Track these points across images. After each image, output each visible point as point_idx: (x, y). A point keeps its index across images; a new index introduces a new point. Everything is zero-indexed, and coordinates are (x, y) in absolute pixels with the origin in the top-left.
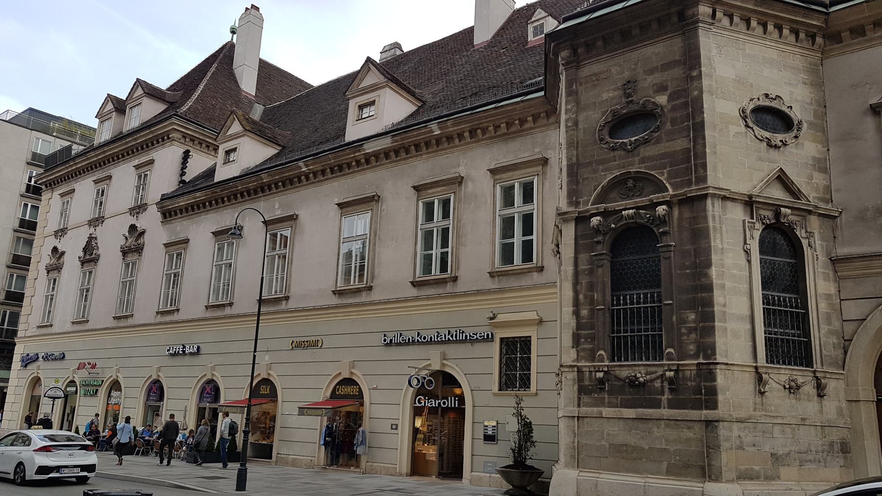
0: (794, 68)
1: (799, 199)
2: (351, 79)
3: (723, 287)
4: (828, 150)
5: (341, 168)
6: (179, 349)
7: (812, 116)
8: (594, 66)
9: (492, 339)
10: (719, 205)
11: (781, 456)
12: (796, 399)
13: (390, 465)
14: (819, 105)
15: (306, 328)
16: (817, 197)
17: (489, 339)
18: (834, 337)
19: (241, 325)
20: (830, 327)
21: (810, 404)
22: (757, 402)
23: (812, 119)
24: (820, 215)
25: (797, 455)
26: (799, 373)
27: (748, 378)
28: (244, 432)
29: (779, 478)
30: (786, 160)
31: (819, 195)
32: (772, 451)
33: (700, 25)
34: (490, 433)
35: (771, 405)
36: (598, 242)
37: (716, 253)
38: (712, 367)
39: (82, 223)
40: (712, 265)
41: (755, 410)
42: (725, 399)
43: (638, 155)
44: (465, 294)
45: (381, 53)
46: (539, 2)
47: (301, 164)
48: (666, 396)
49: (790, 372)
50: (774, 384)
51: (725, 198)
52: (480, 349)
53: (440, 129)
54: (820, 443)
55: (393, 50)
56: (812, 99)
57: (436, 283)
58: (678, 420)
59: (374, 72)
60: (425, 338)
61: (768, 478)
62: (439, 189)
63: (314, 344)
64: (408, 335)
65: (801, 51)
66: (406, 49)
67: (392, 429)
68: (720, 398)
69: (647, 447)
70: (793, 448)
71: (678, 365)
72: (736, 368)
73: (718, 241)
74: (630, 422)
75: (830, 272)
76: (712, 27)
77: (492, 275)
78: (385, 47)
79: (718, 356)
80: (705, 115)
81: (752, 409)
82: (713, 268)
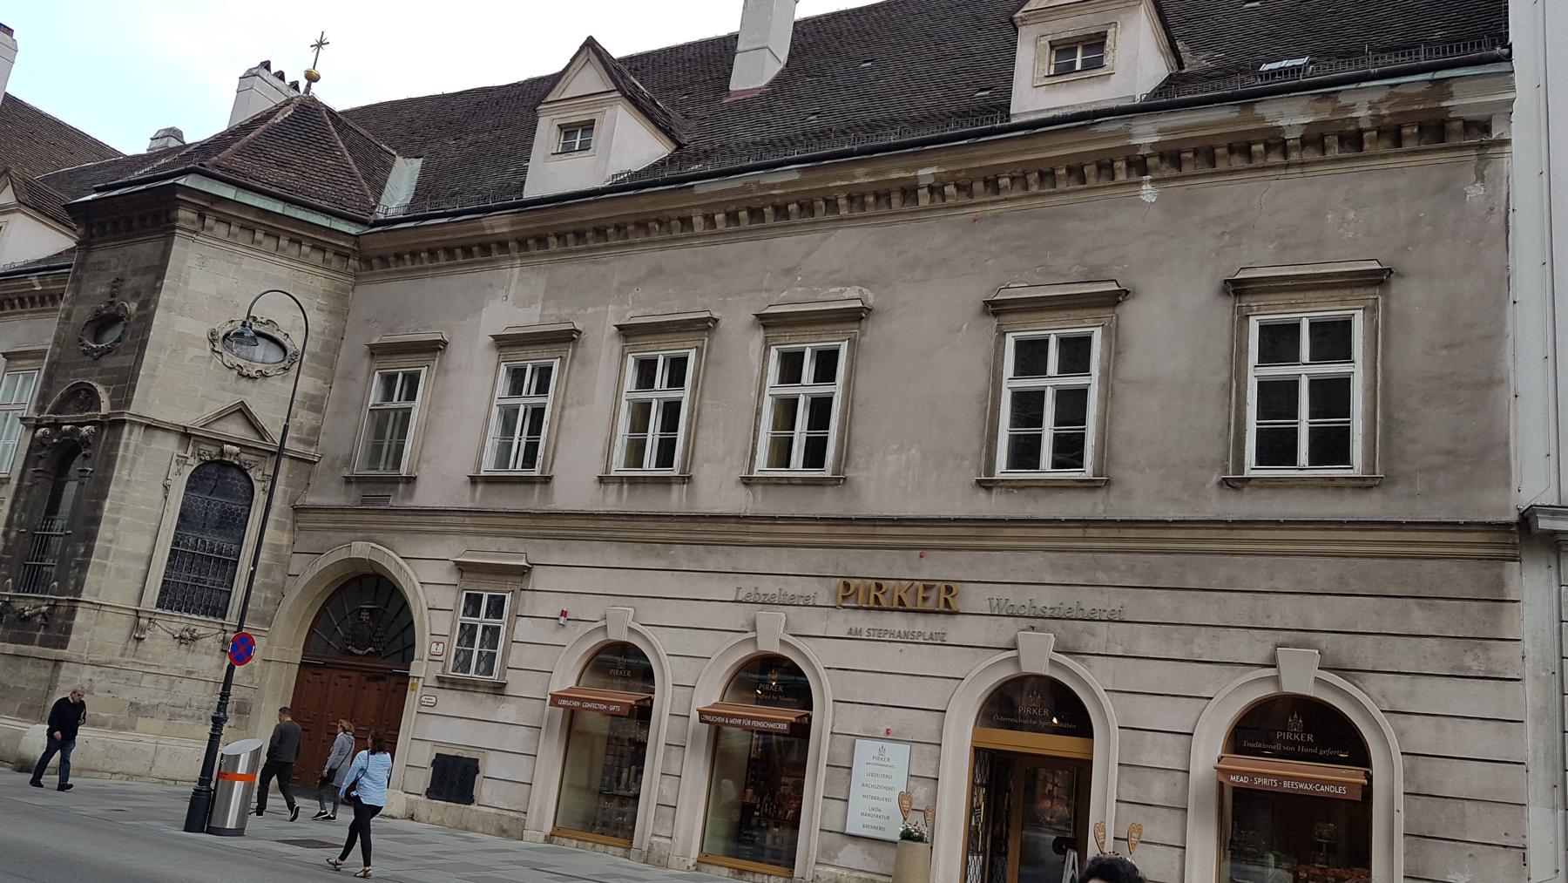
0: (309, 291)
1: (264, 440)
2: (535, 93)
3: (116, 522)
4: (331, 388)
5: (399, 257)
7: (319, 347)
8: (100, 252)
10: (139, 434)
11: (144, 707)
12: (189, 650)
13: (493, 810)
14: (335, 335)
16: (297, 438)
18: (269, 592)
20: (267, 580)
21: (208, 658)
22: (129, 647)
23: (318, 350)
24: (291, 457)
25: (167, 708)
26: (201, 624)
27: (125, 622)
28: (214, 719)
29: (134, 729)
30: (261, 393)
31: (300, 436)
32: (134, 700)
33: (177, 231)
35: (148, 653)
36: (40, 457)
37: (116, 485)
38: (75, 604)
40: (106, 497)
41: (122, 655)
42: (80, 639)
43: (100, 365)
45: (152, 139)
46: (888, 4)
47: (34, 279)
48: (40, 633)
49: (188, 621)
50: (160, 631)
51: (148, 426)
53: (41, 284)
54: (208, 699)
55: (166, 139)
56: (326, 328)
58: (40, 659)
61: (117, 727)
62: (27, 362)
65: (325, 272)
66: (188, 140)
68: (73, 637)
69: (12, 686)
70: (165, 701)
71: (57, 600)
72: (108, 609)
73: (125, 473)
74: (9, 658)
75: (289, 522)
76: (195, 235)
78: (159, 131)
79: (83, 594)
80: (152, 333)
81: (118, 654)
82: (108, 501)
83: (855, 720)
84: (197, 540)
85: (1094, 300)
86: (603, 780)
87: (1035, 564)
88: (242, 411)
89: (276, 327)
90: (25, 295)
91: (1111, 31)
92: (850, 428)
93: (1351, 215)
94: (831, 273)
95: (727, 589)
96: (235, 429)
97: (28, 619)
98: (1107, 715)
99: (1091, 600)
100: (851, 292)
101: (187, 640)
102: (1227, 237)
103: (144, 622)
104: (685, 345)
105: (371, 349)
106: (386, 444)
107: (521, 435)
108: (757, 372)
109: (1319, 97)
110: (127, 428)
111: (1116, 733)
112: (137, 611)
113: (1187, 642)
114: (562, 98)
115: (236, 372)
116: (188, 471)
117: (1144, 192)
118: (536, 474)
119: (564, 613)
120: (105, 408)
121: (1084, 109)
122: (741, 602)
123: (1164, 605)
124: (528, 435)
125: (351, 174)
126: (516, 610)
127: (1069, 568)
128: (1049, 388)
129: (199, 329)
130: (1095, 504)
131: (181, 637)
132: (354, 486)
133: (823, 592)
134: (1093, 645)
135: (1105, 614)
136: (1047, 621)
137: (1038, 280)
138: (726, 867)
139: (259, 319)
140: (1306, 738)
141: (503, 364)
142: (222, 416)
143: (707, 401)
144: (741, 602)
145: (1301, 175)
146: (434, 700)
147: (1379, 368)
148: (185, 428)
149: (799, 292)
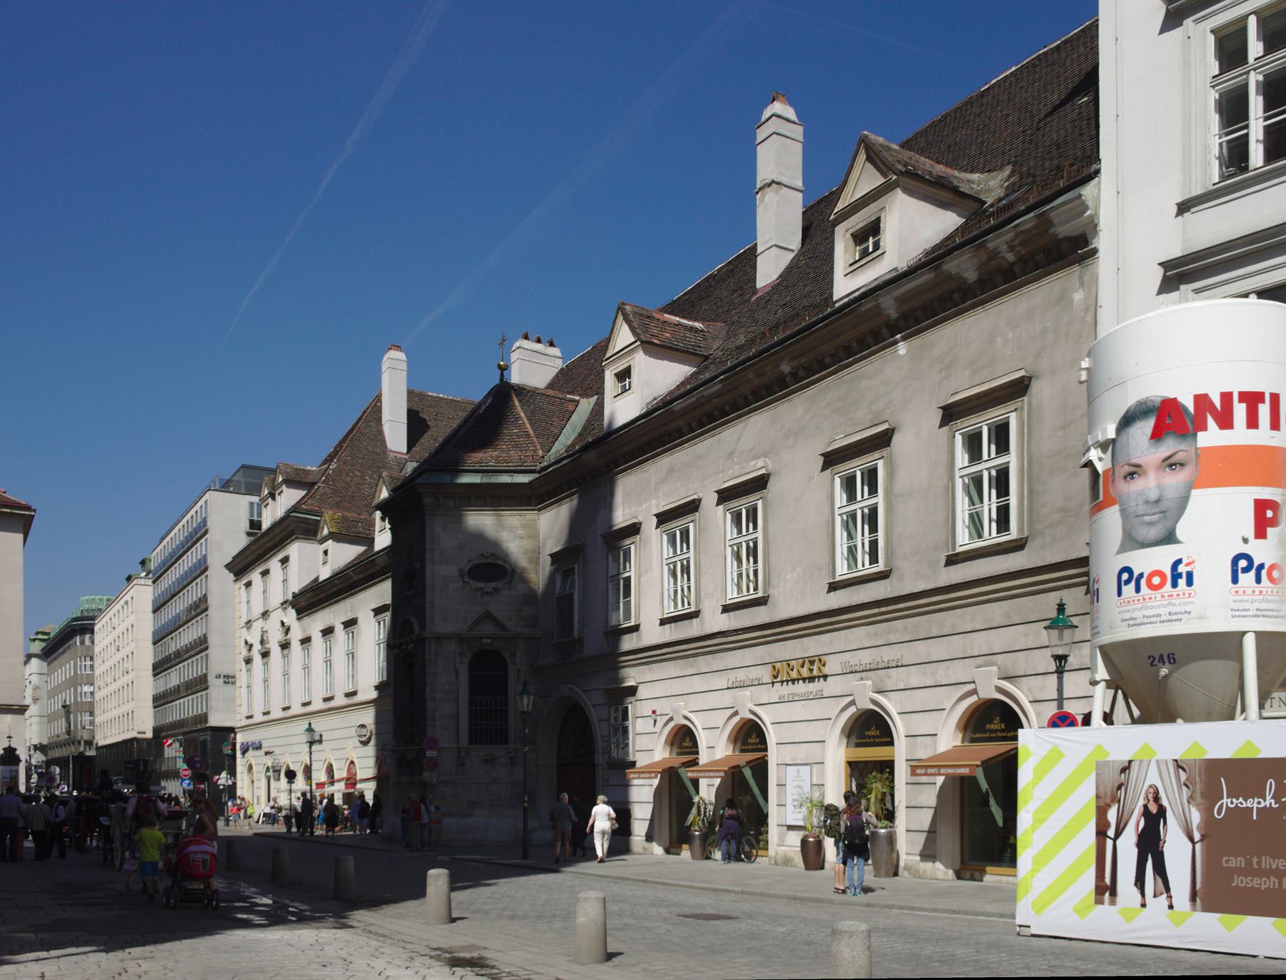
83: (788, 754)
85: (682, 510)
86: (825, 822)
87: (859, 635)
88: (488, 616)
91: (882, 216)
92: (768, 560)
93: (1010, 336)
94: (751, 451)
95: (721, 681)
96: (487, 628)
98: (900, 727)
99: (888, 654)
100: (760, 463)
101: (490, 761)
102: (944, 372)
103: (463, 754)
104: (958, 427)
105: (604, 538)
107: (990, 500)
108: (722, 530)
109: (975, 248)
110: (427, 641)
111: (903, 739)
112: (458, 748)
113: (934, 674)
114: (615, 352)
115: (480, 593)
116: (467, 660)
117: (900, 347)
118: (632, 624)
119: (654, 712)
120: (417, 631)
121: (872, 286)
122: (730, 688)
123: (922, 650)
124: (997, 498)
125: (528, 435)
126: (635, 714)
127: (876, 634)
128: (985, 471)
129: (450, 570)
130: (886, 588)
131: (486, 760)
133: (765, 674)
134: (890, 684)
135: (894, 662)
136: (868, 673)
137: (850, 430)
138: (940, 880)
139: (486, 555)
140: (1001, 727)
141: (836, 476)
142: (477, 622)
143: (702, 557)
144: (730, 688)
145: (983, 310)
146: (607, 777)
147: (1026, 455)
149: (736, 470)
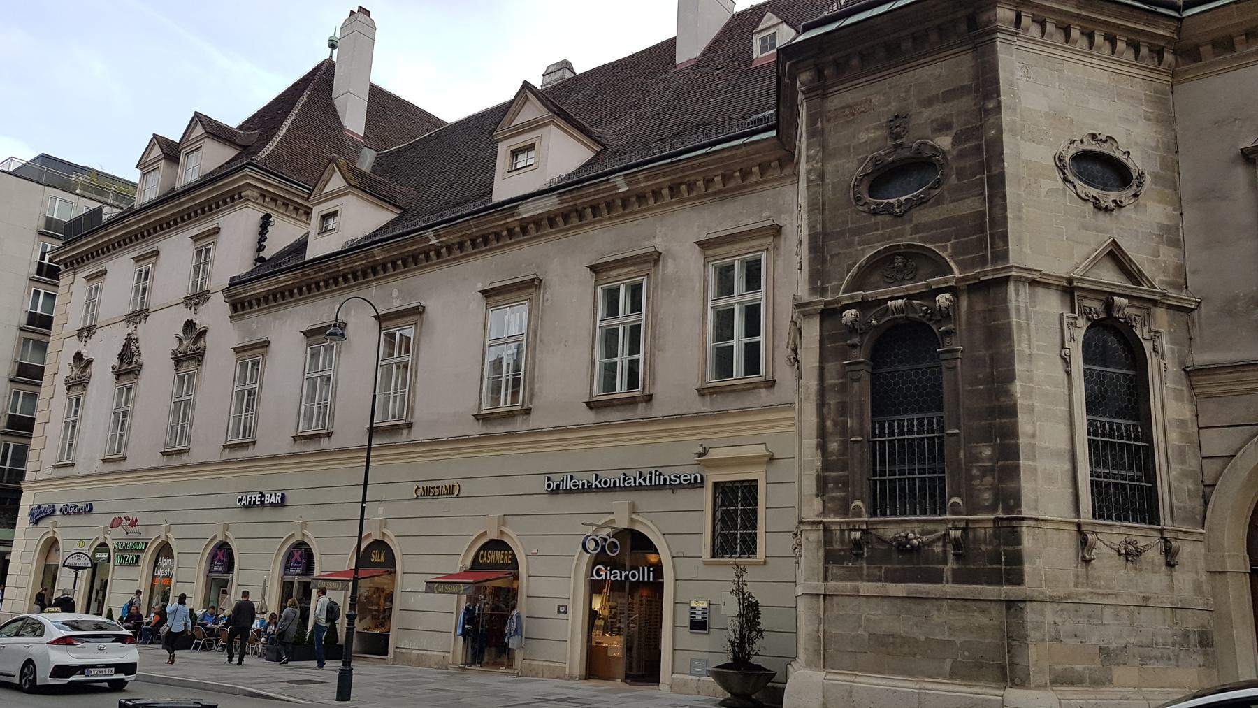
0: (1132, 97)
1: (1140, 284)
2: (500, 113)
4: (1181, 214)
6: (255, 497)
7: (1158, 165)
8: (847, 94)
9: (702, 484)
10: (1025, 293)
11: (1114, 650)
13: (557, 664)
14: (1168, 150)
15: (436, 469)
16: (1166, 281)
17: (697, 484)
18: (1190, 481)
19: (343, 464)
20: (1184, 467)
21: (1156, 577)
22: (1080, 573)
23: (1159, 170)
24: (1170, 307)
25: (1136, 650)
27: (1068, 540)
28: (348, 616)
29: (1111, 682)
30: (1121, 229)
31: (1168, 279)
32: (1101, 644)
33: (999, 35)
34: (699, 618)
35: (1099, 578)
37: (1021, 362)
38: (1015, 524)
39: (116, 318)
40: (1015, 378)
41: (1077, 585)
42: (1034, 569)
43: (911, 221)
44: (664, 420)
45: (543, 75)
48: (950, 565)
49: (1127, 531)
50: (1104, 549)
51: (1033, 283)
52: (685, 499)
53: (628, 184)
54: (1170, 632)
55: (561, 71)
56: (1158, 141)
57: (622, 404)
58: (967, 600)
59: (533, 103)
60: (606, 483)
61: (1096, 682)
62: (626, 270)
63: (448, 492)
64: (582, 479)
65: (1142, 73)
66: (579, 70)
67: (559, 612)
68: (1027, 567)
69: (923, 639)
70: (1131, 640)
71: (967, 521)
72: (1049, 525)
73: (1024, 345)
74: (899, 602)
75: (1184, 388)
77: (701, 392)
78: (549, 67)
79: (1024, 509)
80: (1006, 164)
81: (1072, 584)
82: (1017, 383)
84: (1105, 424)
89: (1115, 144)
90: (357, 268)
97: (918, 549)
106: (504, 379)
132: (640, 405)
148: (1070, 281)
